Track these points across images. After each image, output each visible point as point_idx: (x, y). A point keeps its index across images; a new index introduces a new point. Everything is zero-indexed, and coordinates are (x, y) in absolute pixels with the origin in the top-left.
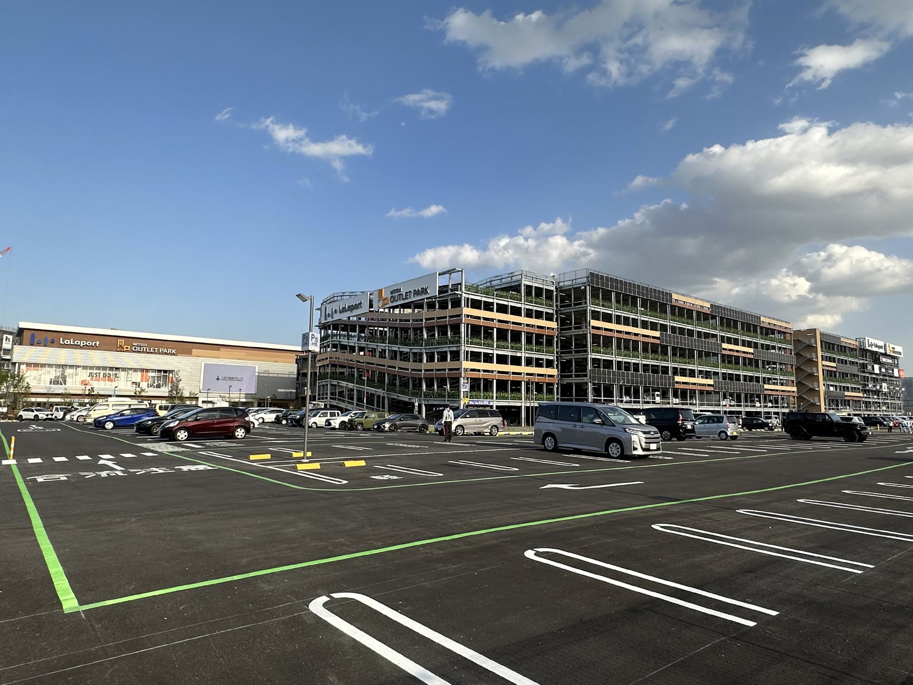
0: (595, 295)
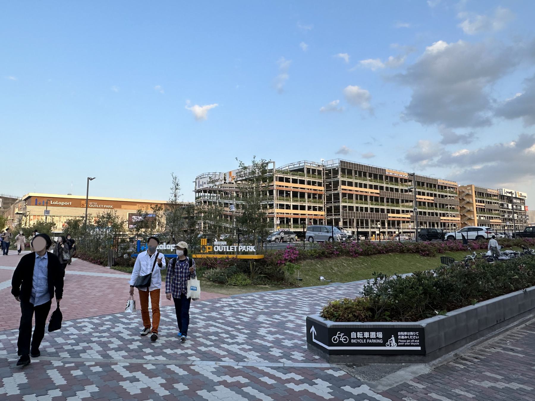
0: (343, 170)
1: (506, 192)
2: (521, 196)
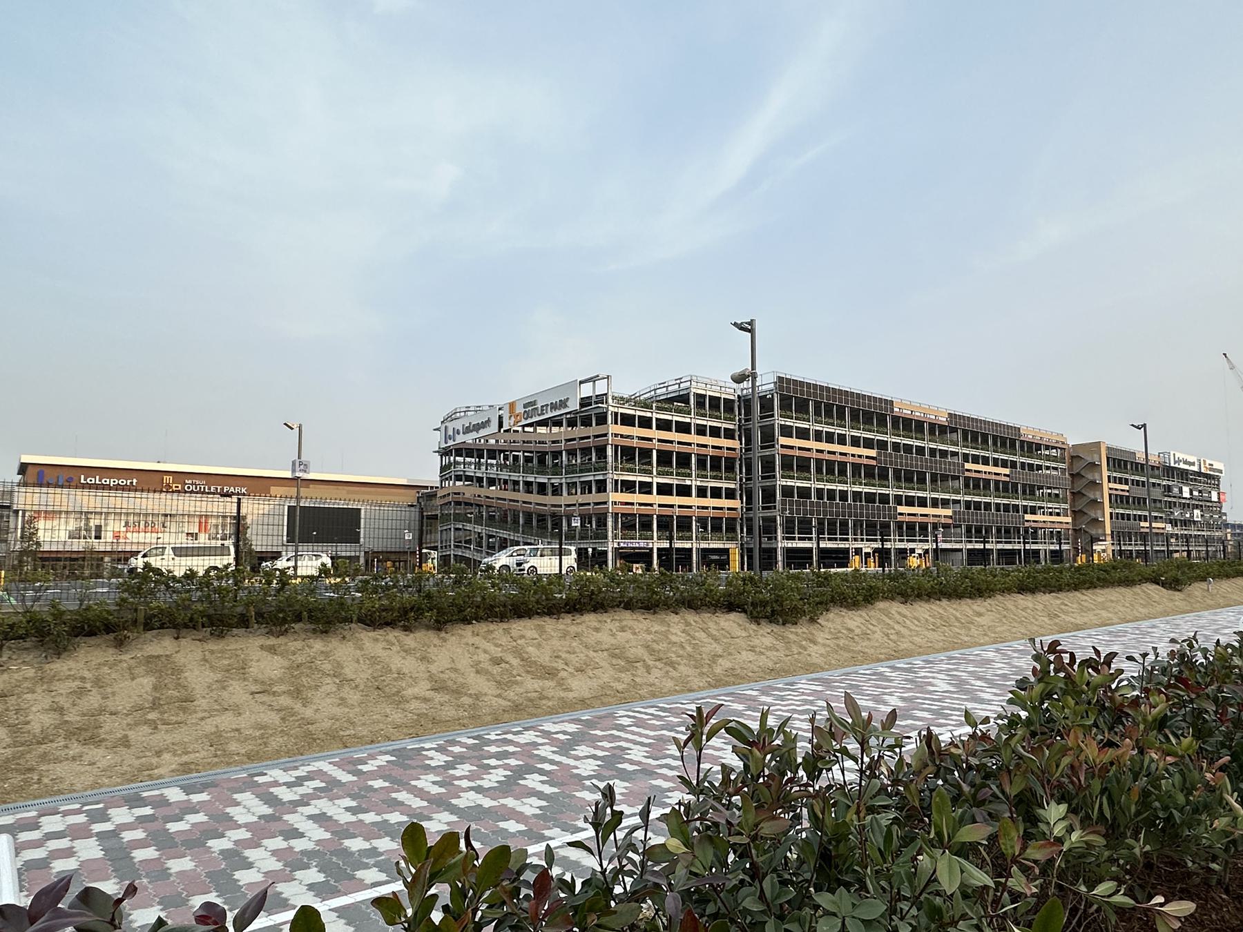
0: (785, 405)
1: (1177, 459)
2: (1211, 470)
